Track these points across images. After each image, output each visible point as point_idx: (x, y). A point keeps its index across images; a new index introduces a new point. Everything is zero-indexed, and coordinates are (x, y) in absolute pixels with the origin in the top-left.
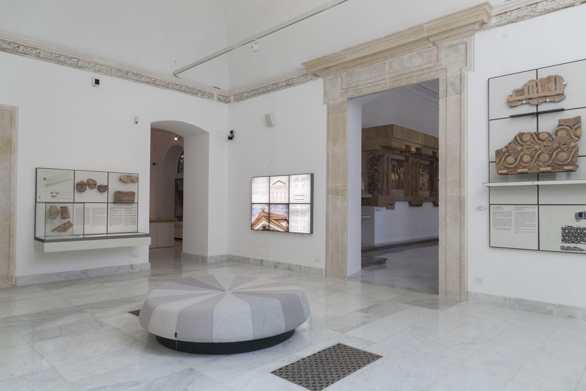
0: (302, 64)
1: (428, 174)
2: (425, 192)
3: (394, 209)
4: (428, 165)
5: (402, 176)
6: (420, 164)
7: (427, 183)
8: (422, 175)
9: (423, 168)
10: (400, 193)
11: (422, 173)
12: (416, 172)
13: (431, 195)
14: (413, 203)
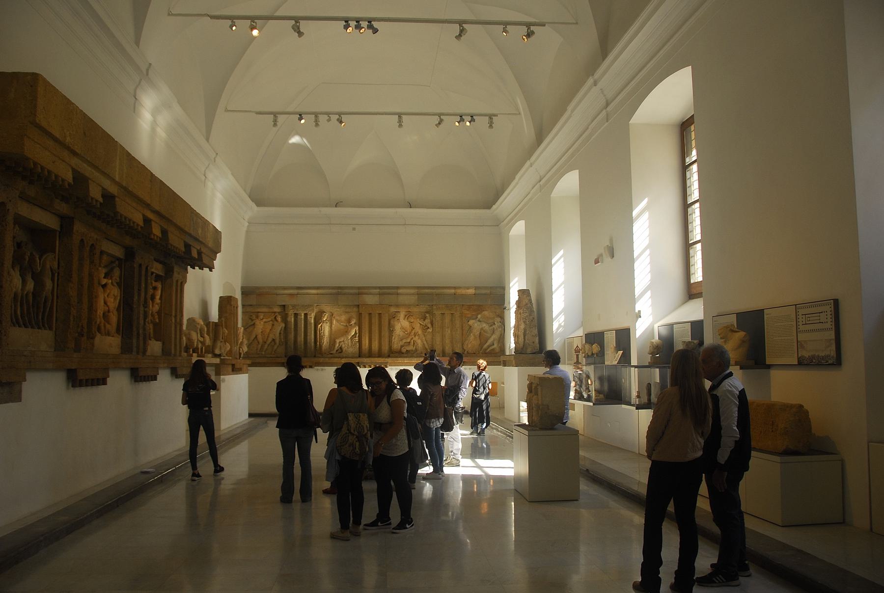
0: (639, 311)
1: (119, 285)
2: (109, 339)
3: (19, 399)
4: (119, 259)
5: (49, 284)
6: (102, 252)
7: (116, 313)
8: (104, 286)
9: (106, 266)
10: (41, 340)
11: (104, 281)
12: (91, 275)
13: (126, 348)
14: (81, 375)
